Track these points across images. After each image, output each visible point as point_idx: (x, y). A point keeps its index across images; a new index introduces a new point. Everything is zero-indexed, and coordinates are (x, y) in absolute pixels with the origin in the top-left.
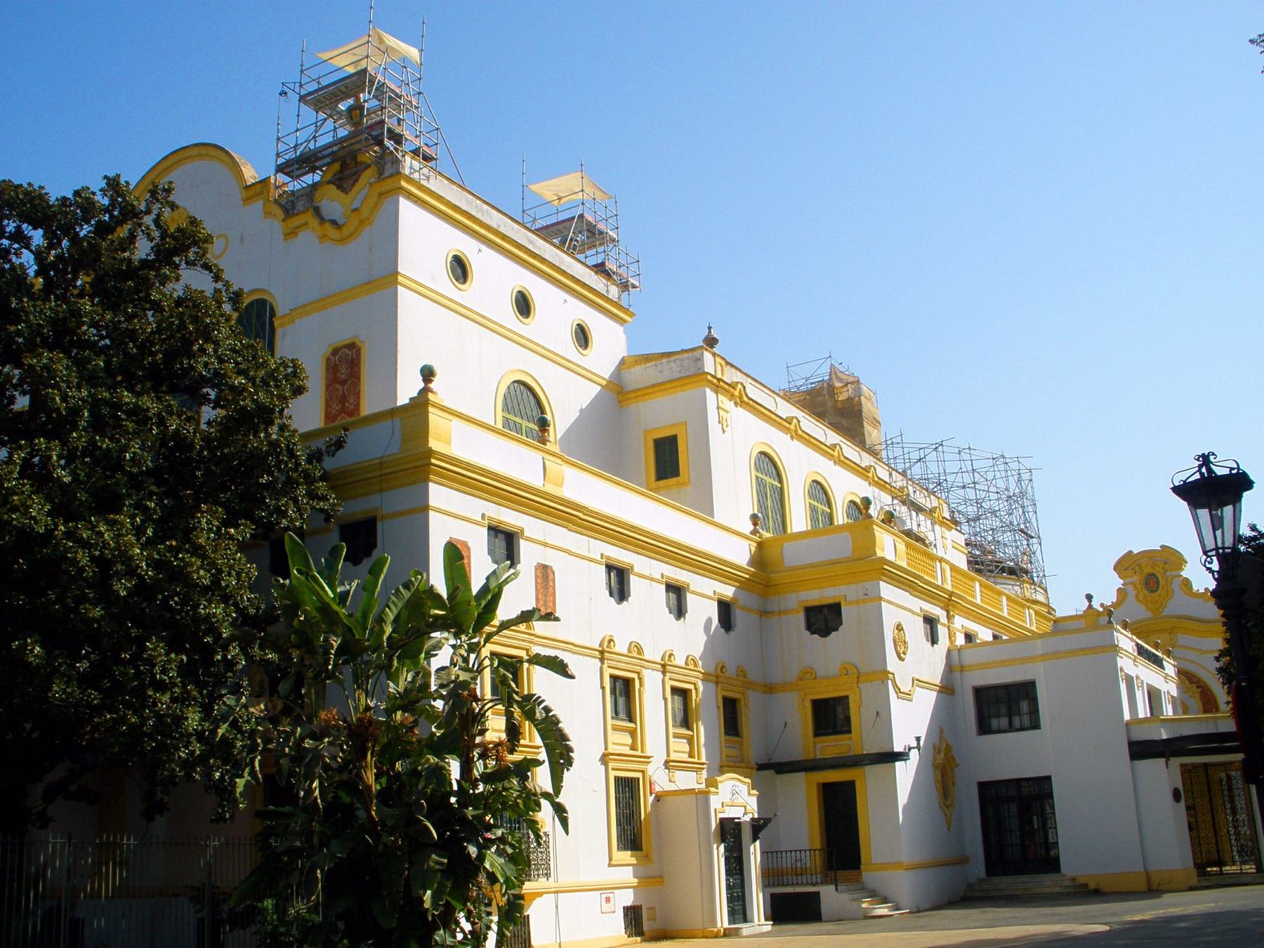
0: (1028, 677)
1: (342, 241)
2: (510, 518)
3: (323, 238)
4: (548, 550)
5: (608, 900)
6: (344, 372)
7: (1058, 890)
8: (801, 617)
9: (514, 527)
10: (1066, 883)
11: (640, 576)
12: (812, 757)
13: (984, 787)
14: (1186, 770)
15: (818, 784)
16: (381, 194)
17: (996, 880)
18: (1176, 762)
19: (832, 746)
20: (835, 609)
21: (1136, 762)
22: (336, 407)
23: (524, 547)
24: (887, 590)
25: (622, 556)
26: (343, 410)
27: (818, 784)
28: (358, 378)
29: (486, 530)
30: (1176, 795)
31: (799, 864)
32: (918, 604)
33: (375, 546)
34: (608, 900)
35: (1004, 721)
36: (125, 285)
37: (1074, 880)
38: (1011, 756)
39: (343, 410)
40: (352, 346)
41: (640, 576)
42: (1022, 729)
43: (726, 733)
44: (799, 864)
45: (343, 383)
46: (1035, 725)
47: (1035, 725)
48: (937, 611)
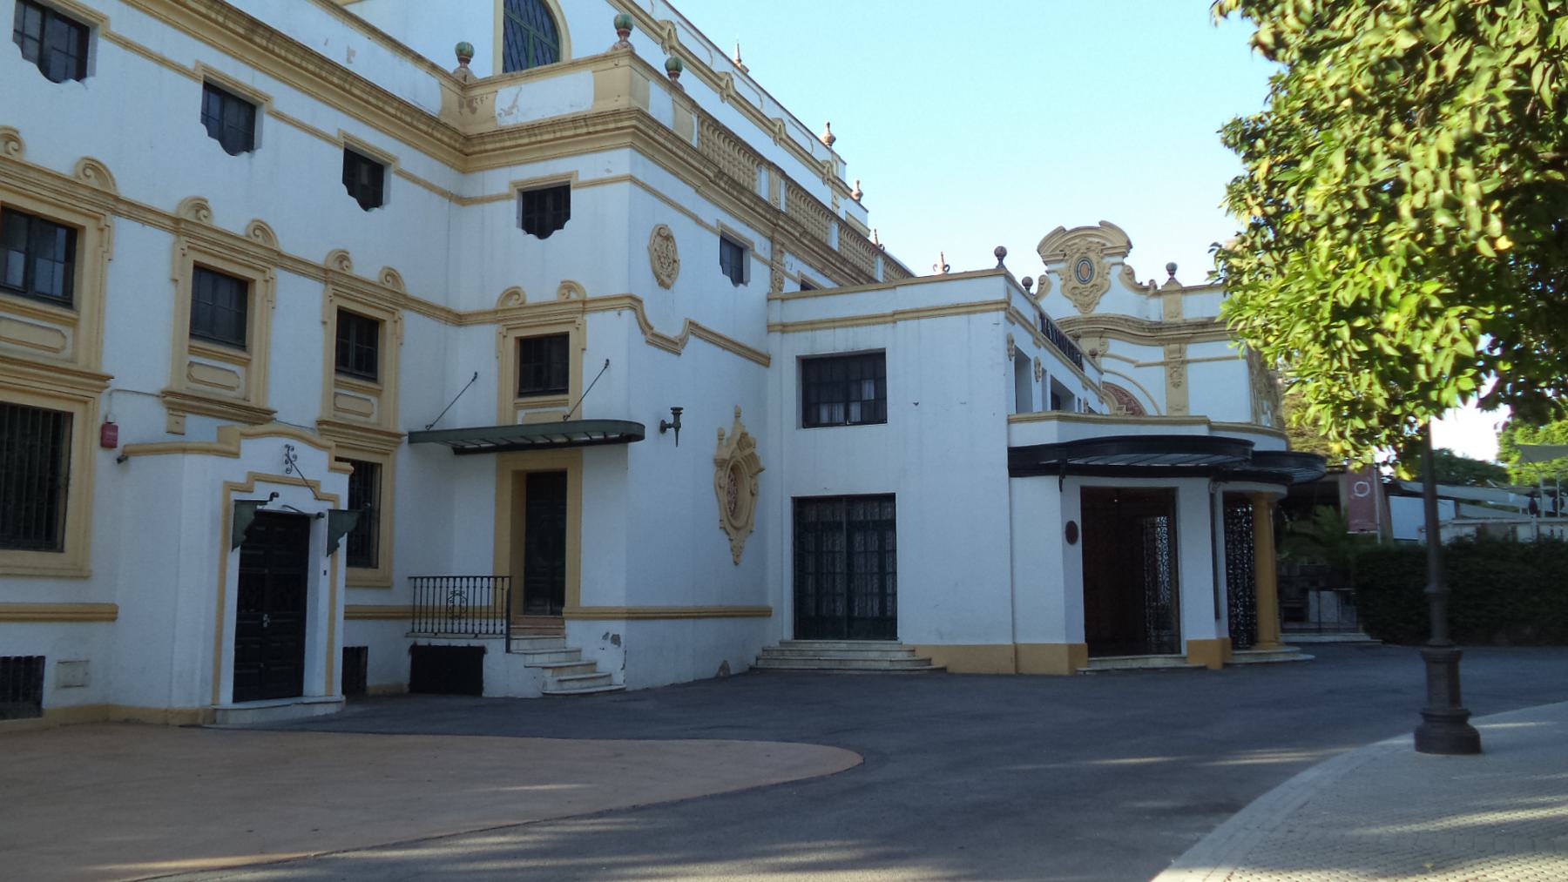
8: (511, 210)
9: (255, 92)
14: (1087, 495)
15: (62, 550)
18: (1075, 483)
19: (544, 412)
20: (872, 363)
21: (1017, 481)
24: (786, 280)
25: (374, 140)
27: (62, 550)
29: (201, 86)
30: (1070, 533)
31: (457, 602)
32: (712, 214)
35: (839, 413)
37: (929, 661)
38: (843, 461)
43: (338, 371)
44: (457, 602)
48: (759, 244)
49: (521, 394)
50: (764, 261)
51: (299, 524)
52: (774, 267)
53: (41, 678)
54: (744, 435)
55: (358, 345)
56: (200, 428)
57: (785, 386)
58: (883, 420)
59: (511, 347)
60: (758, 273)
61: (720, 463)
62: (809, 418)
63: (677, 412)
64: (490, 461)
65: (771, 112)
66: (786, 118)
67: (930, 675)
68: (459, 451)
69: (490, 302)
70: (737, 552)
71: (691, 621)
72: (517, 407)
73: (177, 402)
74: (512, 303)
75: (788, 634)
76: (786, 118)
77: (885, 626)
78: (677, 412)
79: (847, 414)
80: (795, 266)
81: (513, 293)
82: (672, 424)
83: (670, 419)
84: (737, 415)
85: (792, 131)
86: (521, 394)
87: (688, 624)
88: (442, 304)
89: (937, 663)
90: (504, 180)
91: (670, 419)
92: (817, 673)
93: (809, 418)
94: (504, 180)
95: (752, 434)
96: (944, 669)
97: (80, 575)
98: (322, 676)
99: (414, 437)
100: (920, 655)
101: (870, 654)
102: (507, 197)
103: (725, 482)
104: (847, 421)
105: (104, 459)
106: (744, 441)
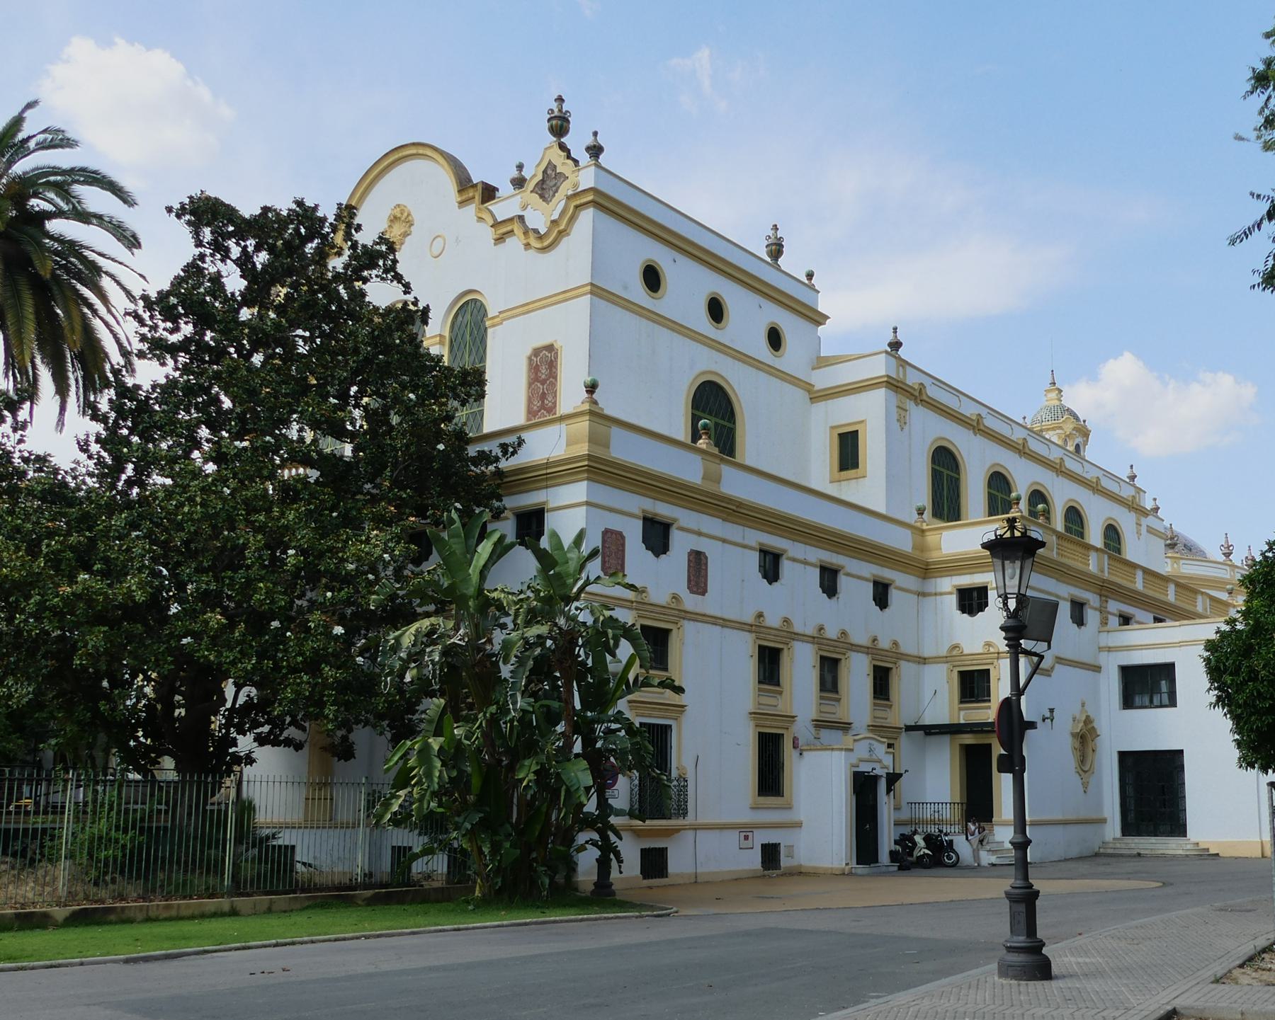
0: (357, 753)
1: (544, 250)
2: (663, 510)
3: (527, 246)
4: (702, 538)
5: (746, 838)
6: (544, 371)
7: (1181, 852)
8: (953, 599)
10: (1189, 847)
11: (794, 560)
12: (956, 722)
13: (1123, 755)
16: (576, 207)
17: (1129, 839)
22: (537, 403)
23: (676, 537)
25: (775, 542)
26: (543, 407)
28: (555, 378)
33: (427, 560)
34: (746, 838)
35: (1146, 700)
36: (331, 307)
39: (543, 407)
40: (550, 348)
41: (794, 560)
42: (1161, 706)
45: (543, 382)
46: (1173, 703)
47: (1173, 703)
48: (1091, 598)
49: (961, 702)
50: (1096, 609)
51: (875, 779)
52: (1102, 610)
53: (1155, 833)
54: (1088, 717)
55: (882, 682)
56: (825, 734)
57: (1111, 685)
58: (1182, 751)
59: (955, 676)
60: (1092, 616)
61: (1074, 735)
62: (1128, 703)
63: (1052, 711)
64: (946, 738)
65: (969, 410)
66: (984, 412)
67: (1206, 856)
68: (927, 734)
69: (943, 651)
70: (1085, 786)
71: (716, 833)
72: (960, 709)
73: (820, 724)
74: (955, 653)
75: (1118, 833)
76: (984, 412)
77: (1178, 828)
78: (1052, 711)
79: (1151, 701)
80: (1114, 606)
81: (956, 647)
82: (1050, 716)
83: (1048, 715)
84: (1083, 705)
85: (990, 422)
86: (961, 702)
87: (1060, 828)
88: (916, 654)
89: (1212, 852)
90: (948, 584)
91: (1048, 715)
92: (1157, 857)
93: (1128, 703)
94: (948, 584)
95: (1092, 717)
96: (1217, 855)
97: (789, 807)
98: (884, 857)
99: (909, 728)
100: (1202, 846)
101: (1170, 846)
102: (950, 593)
103: (1077, 745)
104: (1151, 705)
105: (795, 753)
106: (1088, 721)
